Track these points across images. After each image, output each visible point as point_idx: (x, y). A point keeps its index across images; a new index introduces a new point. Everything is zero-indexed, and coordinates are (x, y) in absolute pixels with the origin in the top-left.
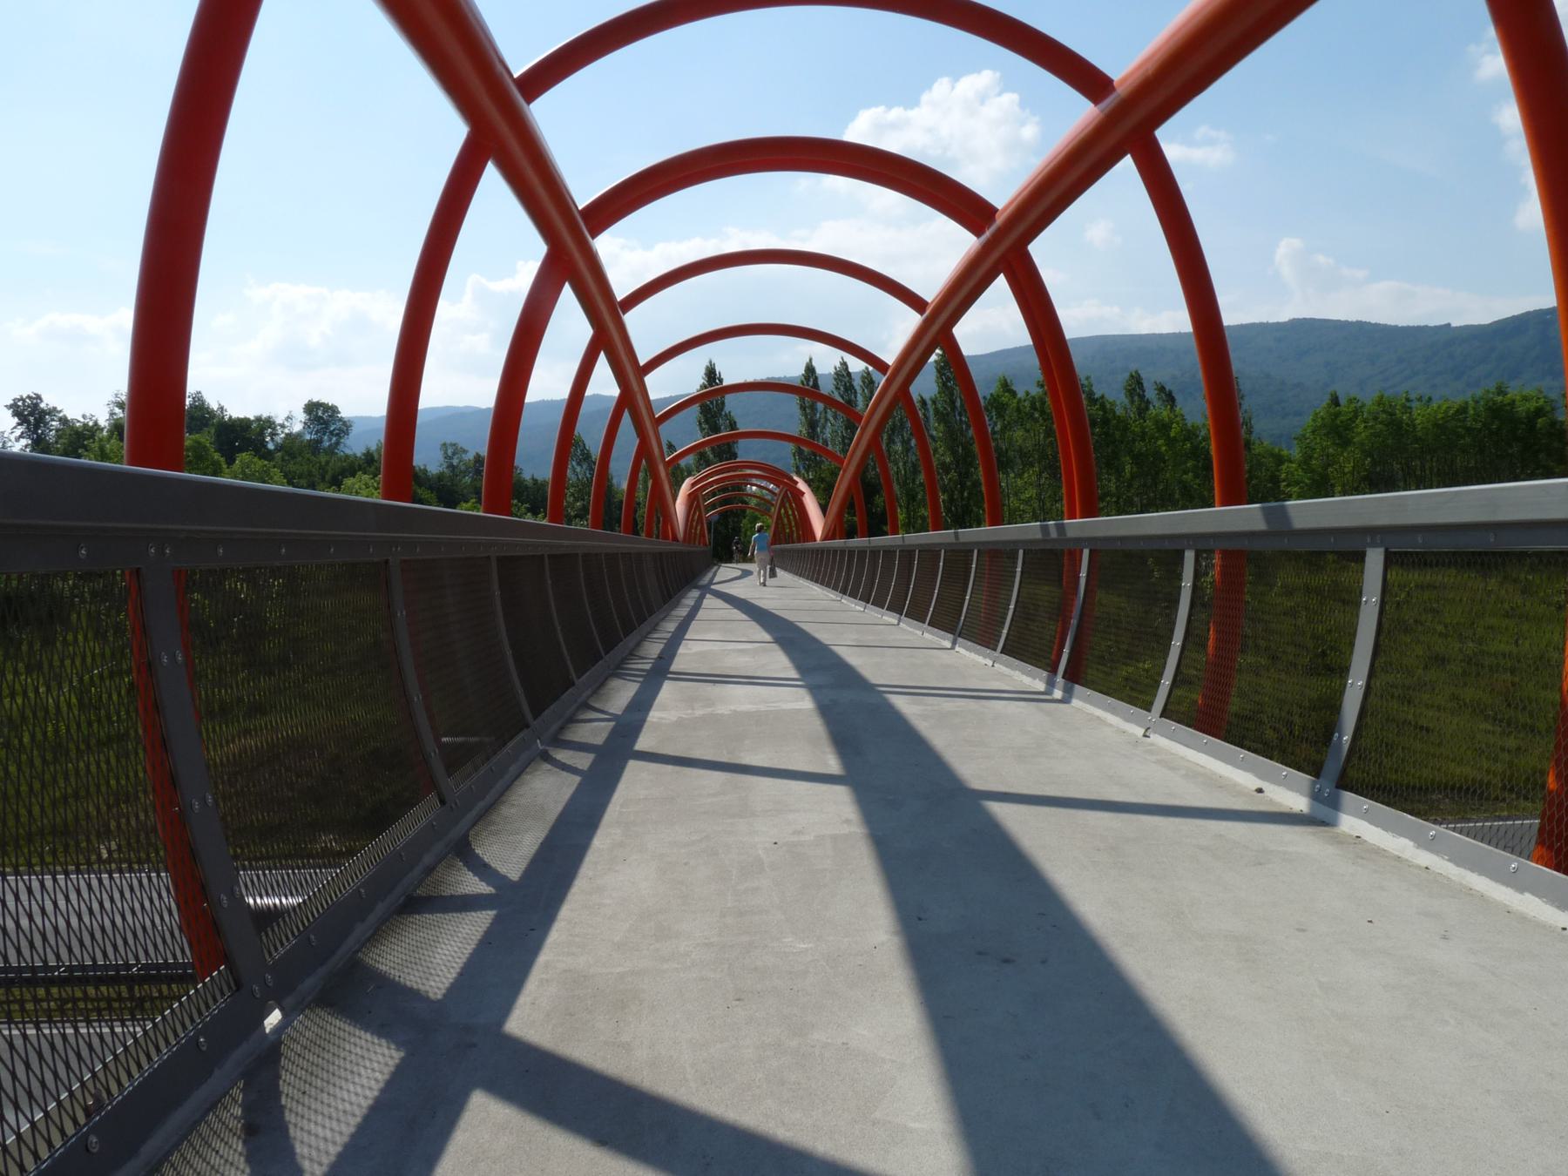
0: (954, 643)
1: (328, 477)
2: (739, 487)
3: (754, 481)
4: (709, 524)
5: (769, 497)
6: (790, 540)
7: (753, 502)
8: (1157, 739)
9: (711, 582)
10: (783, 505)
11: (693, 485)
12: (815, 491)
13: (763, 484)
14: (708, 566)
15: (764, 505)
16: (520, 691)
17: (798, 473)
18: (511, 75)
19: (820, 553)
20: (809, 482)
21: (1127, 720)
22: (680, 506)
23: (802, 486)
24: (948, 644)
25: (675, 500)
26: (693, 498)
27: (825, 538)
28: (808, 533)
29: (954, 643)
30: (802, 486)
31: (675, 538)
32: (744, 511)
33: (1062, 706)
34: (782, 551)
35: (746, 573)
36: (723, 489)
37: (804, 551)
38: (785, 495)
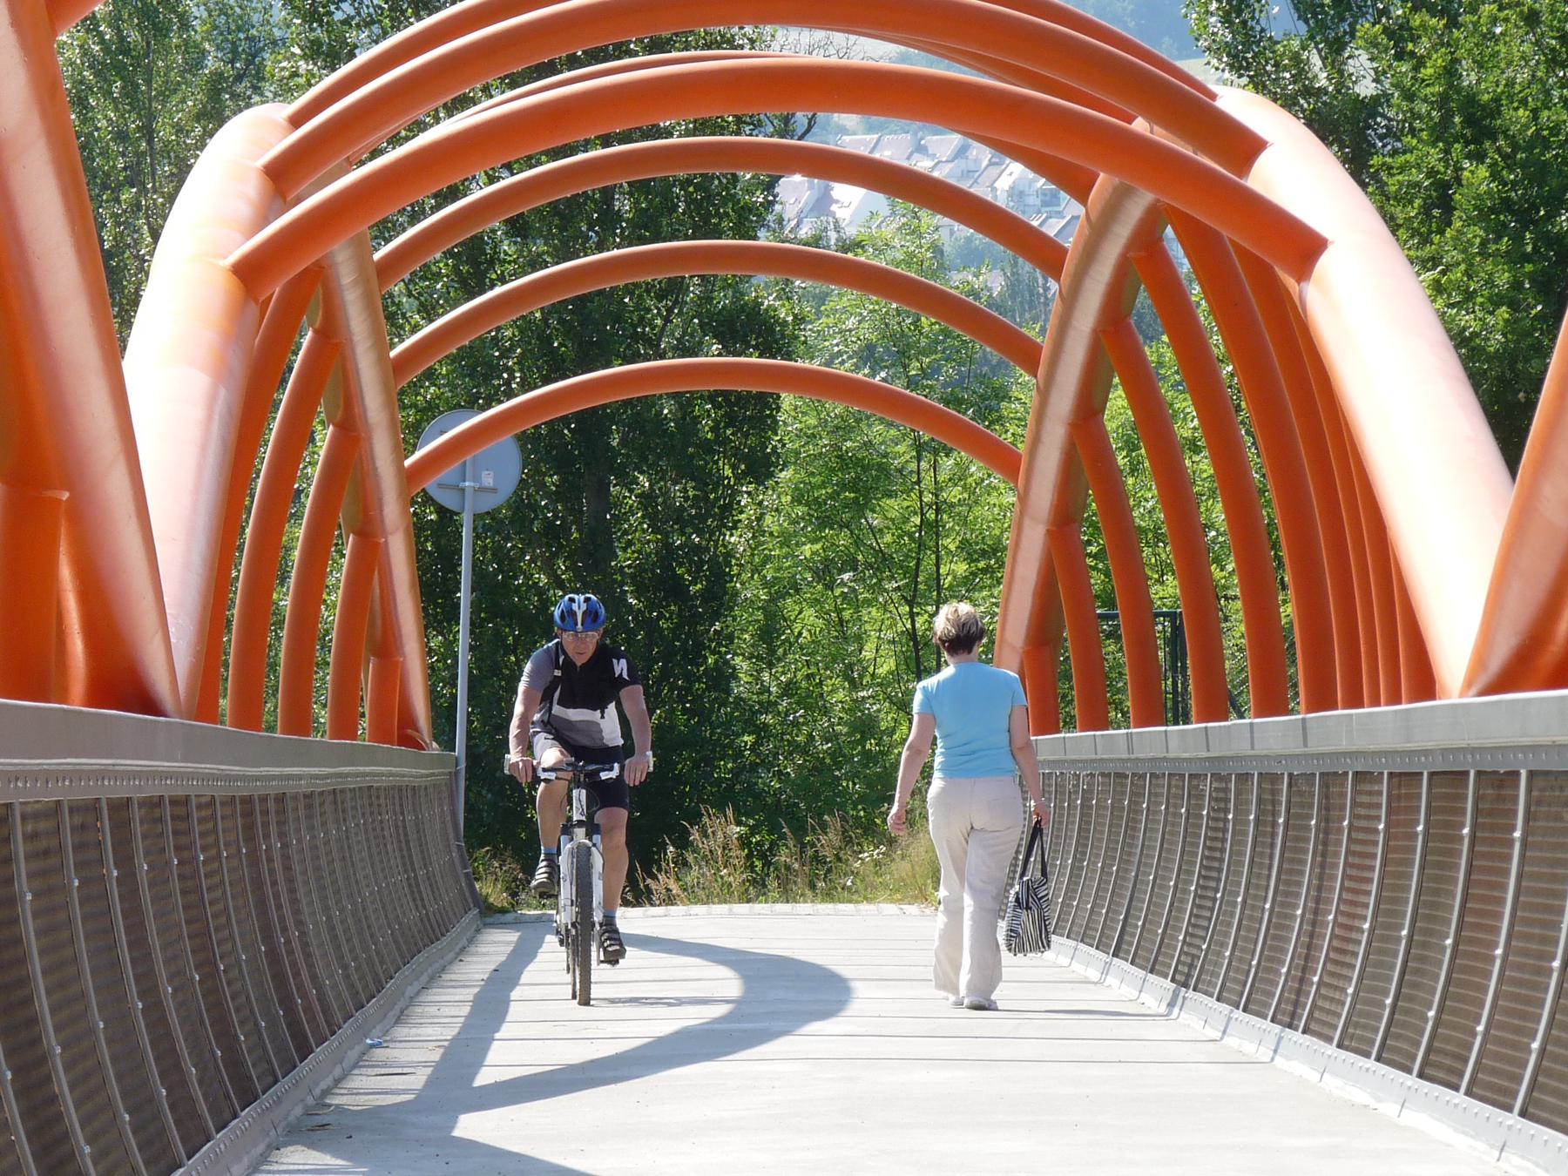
0: (1106, 971)
1: (423, 793)
2: (713, 202)
3: (851, 133)
4: (436, 538)
5: (987, 277)
6: (1177, 677)
7: (839, 326)
8: (1411, 1118)
9: (456, 1083)
10: (1115, 346)
11: (283, 175)
12: (1419, 219)
13: (940, 152)
14: (416, 940)
15: (954, 353)
16: (1362, 649)
17: (1248, 57)
18: (951, 935)
19: (1466, 796)
20: (1346, 130)
21: (973, 919)
22: (164, 394)
23: (1297, 172)
24: (1094, 974)
25: (117, 288)
26: (278, 289)
27: (1528, 662)
28: (1348, 613)
29: (1106, 971)
30: (1297, 172)
31: (120, 685)
32: (751, 412)
33: (1161, 1022)
34: (1123, 780)
35: (788, 996)
36: (566, 219)
37: (1328, 786)
38: (1145, 255)
